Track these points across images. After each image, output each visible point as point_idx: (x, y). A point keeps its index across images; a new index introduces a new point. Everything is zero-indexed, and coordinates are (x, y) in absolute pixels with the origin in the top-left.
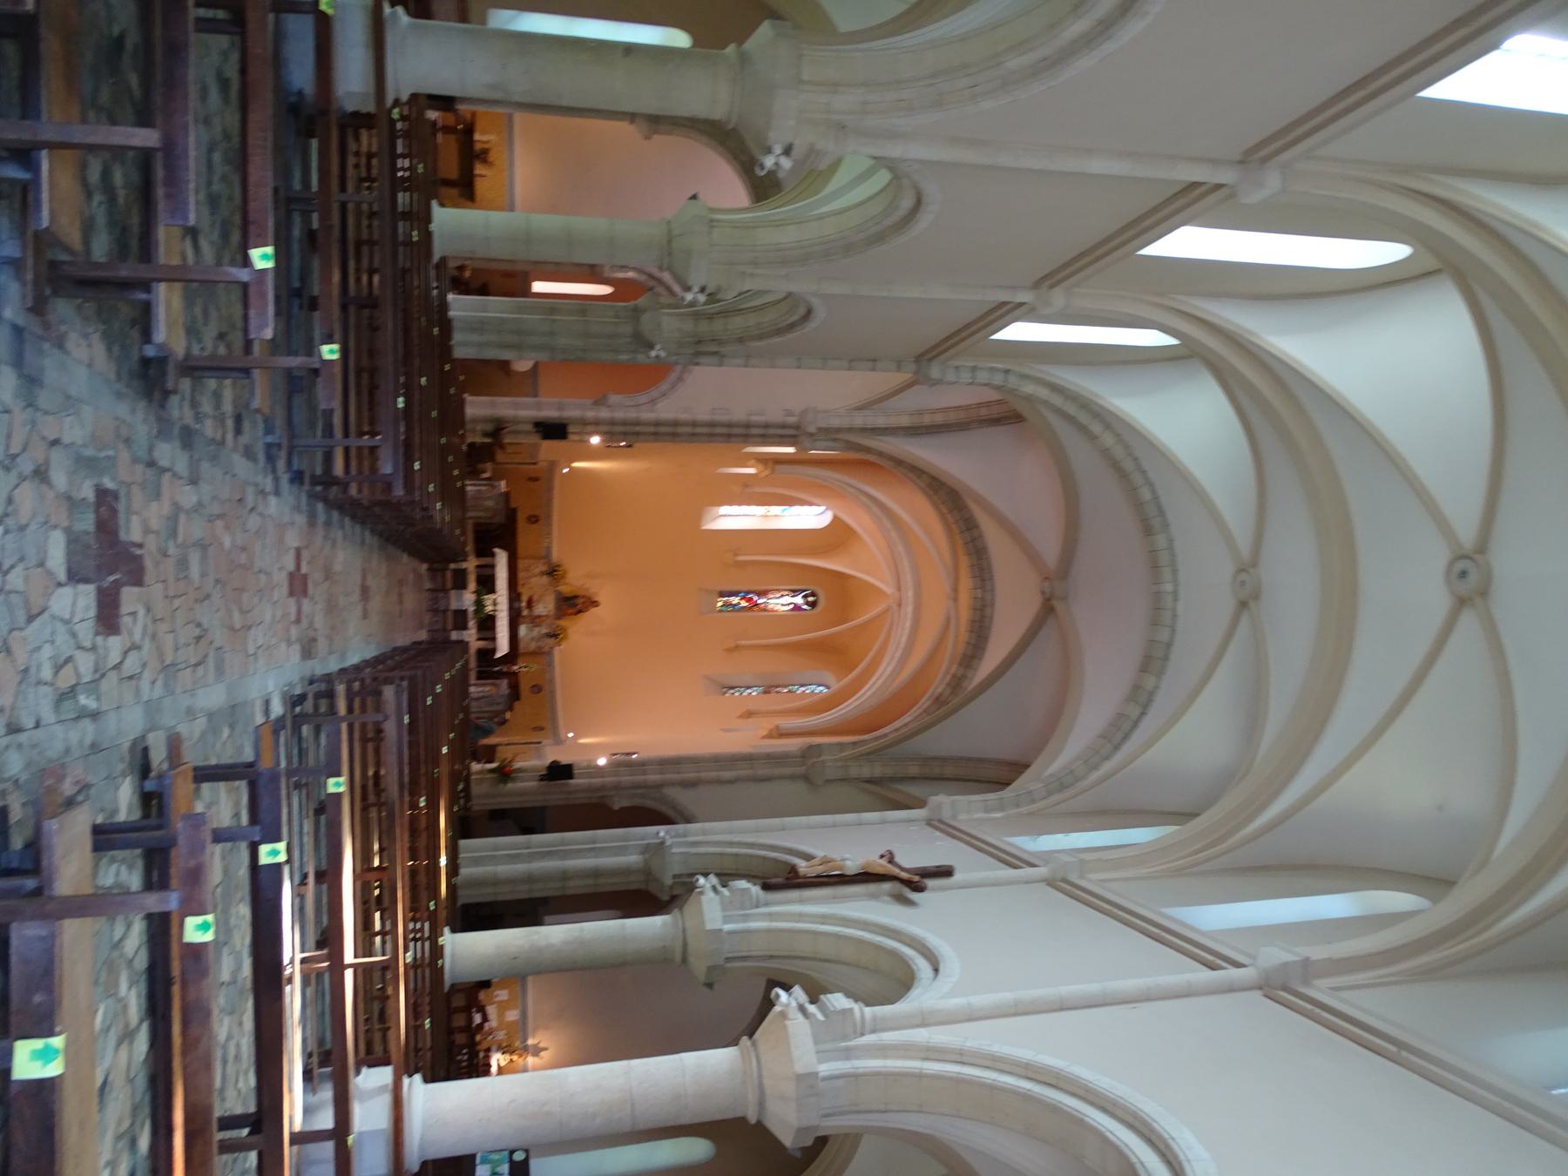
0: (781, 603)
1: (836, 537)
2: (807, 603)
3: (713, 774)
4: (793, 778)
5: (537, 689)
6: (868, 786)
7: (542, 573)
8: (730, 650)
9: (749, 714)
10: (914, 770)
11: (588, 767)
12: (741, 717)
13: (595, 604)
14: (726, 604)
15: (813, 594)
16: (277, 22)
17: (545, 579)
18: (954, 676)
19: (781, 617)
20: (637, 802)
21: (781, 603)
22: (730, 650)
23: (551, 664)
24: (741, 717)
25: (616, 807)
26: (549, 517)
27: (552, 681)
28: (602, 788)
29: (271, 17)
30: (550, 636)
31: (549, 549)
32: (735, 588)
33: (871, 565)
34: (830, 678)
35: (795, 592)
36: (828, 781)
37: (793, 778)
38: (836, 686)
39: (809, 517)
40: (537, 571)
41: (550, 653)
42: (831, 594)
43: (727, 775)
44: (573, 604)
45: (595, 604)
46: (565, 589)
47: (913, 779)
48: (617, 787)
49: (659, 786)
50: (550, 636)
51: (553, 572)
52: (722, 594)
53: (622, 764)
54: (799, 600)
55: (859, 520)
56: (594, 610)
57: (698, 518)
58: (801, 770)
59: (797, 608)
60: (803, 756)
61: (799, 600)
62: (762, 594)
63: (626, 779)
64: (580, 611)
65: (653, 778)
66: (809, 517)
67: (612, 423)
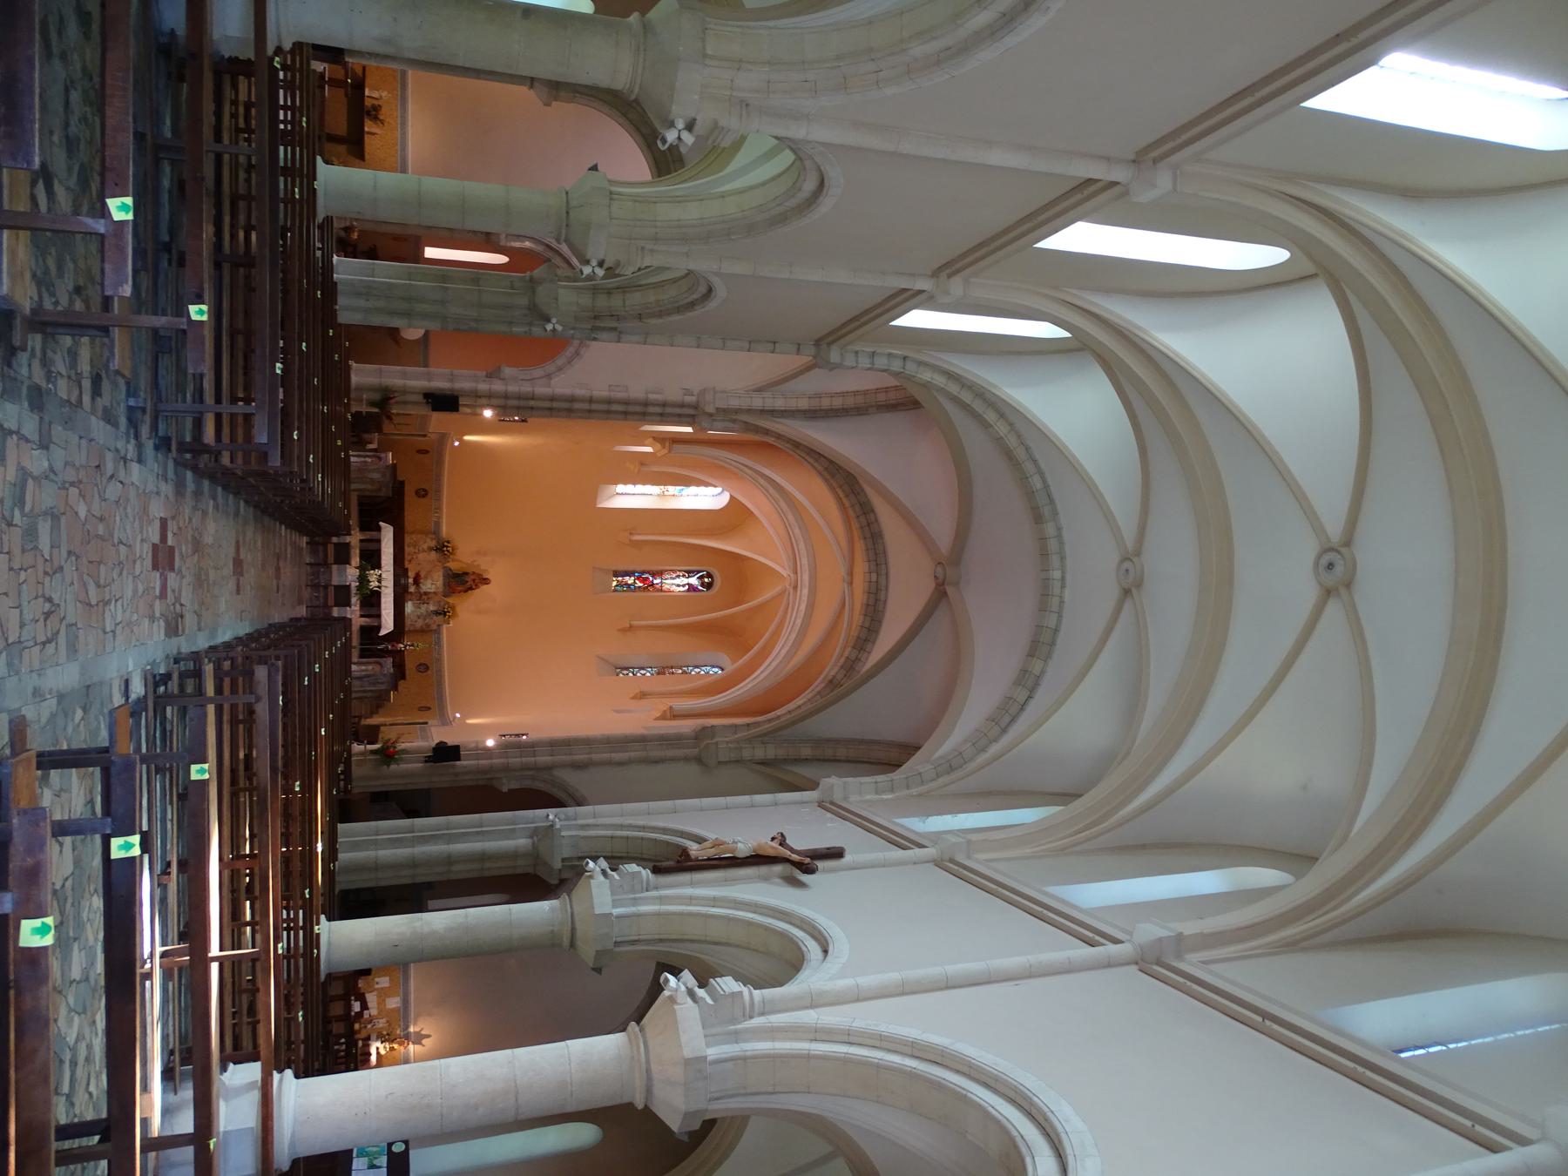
0: (676, 584)
1: (732, 518)
5: (423, 668)
6: (762, 768)
7: (431, 549)
9: (643, 695)
10: (806, 752)
12: (634, 698)
13: (486, 581)
14: (620, 584)
15: (709, 575)
19: (676, 598)
20: (527, 784)
21: (676, 584)
23: (439, 642)
24: (634, 698)
25: (505, 789)
26: (439, 491)
27: (439, 660)
28: (491, 769)
30: (437, 613)
31: (438, 524)
32: (631, 568)
33: (766, 547)
34: (724, 659)
35: (690, 573)
37: (686, 759)
38: (730, 667)
39: (706, 498)
41: (438, 631)
42: (725, 576)
43: (617, 756)
44: (463, 581)
45: (486, 581)
48: (506, 769)
49: (549, 768)
50: (437, 613)
51: (443, 548)
52: (616, 574)
54: (694, 581)
55: (756, 502)
59: (692, 588)
61: (694, 581)
63: (515, 761)
65: (544, 759)
66: (706, 498)
67: (506, 396)
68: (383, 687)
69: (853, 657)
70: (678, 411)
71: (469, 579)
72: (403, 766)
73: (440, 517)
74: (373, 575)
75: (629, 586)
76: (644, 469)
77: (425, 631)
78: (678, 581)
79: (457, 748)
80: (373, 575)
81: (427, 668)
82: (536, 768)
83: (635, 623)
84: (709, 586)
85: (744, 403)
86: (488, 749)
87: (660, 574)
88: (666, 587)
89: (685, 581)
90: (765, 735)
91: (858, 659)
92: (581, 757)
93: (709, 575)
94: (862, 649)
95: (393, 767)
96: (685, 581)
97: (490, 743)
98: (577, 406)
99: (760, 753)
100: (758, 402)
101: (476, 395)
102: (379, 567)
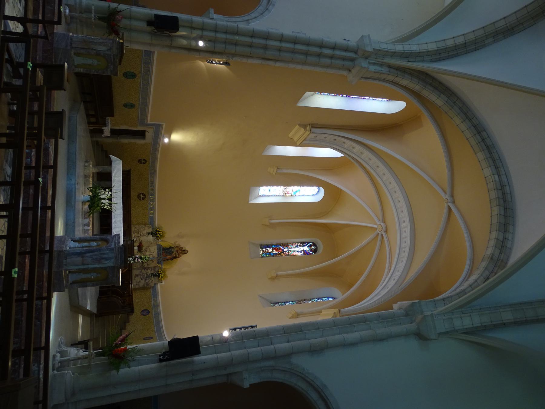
0: (296, 251)
2: (311, 250)
3: (339, 337)
4: (406, 335)
5: (146, 312)
6: (464, 337)
7: (148, 234)
8: (273, 279)
10: (508, 316)
11: (218, 338)
13: (185, 252)
14: (264, 253)
15: (314, 245)
16: (5, 23)
17: (151, 238)
18: (497, 239)
20: (267, 376)
21: (296, 251)
22: (273, 279)
23: (155, 296)
25: (246, 385)
26: (153, 194)
27: (156, 306)
28: (231, 363)
29: (3, 21)
30: (153, 275)
31: (152, 218)
32: (269, 242)
33: (359, 212)
35: (303, 244)
36: (439, 334)
37: (406, 335)
40: (145, 232)
41: (154, 288)
43: (351, 336)
44: (171, 254)
45: (185, 252)
46: (164, 245)
47: (504, 325)
48: (246, 361)
49: (288, 355)
50: (153, 275)
51: (156, 234)
52: (262, 247)
53: (246, 336)
54: (306, 248)
56: (184, 257)
57: (247, 194)
58: (413, 327)
60: (407, 315)
61: (306, 248)
62: (284, 246)
63: (254, 350)
64: (176, 257)
65: (283, 346)
67: (216, 29)
68: (109, 264)
69: (501, 238)
70: (344, 54)
71: (174, 251)
72: (136, 369)
73: (154, 214)
74: (104, 194)
75: (270, 253)
76: (279, 171)
77: (145, 288)
78: (297, 249)
79: (195, 340)
80: (104, 194)
81: (148, 312)
82: (276, 357)
83: (279, 273)
84: (315, 251)
85: (391, 47)
86: (225, 341)
87: (286, 245)
88: (291, 253)
89: (302, 249)
90: (461, 307)
91: (504, 239)
92: (317, 341)
93: (314, 245)
94: (505, 232)
95: (124, 371)
96: (302, 249)
97: (226, 334)
98: (271, 43)
99: (467, 322)
100: (399, 48)
101: (192, 27)
102: (110, 188)
